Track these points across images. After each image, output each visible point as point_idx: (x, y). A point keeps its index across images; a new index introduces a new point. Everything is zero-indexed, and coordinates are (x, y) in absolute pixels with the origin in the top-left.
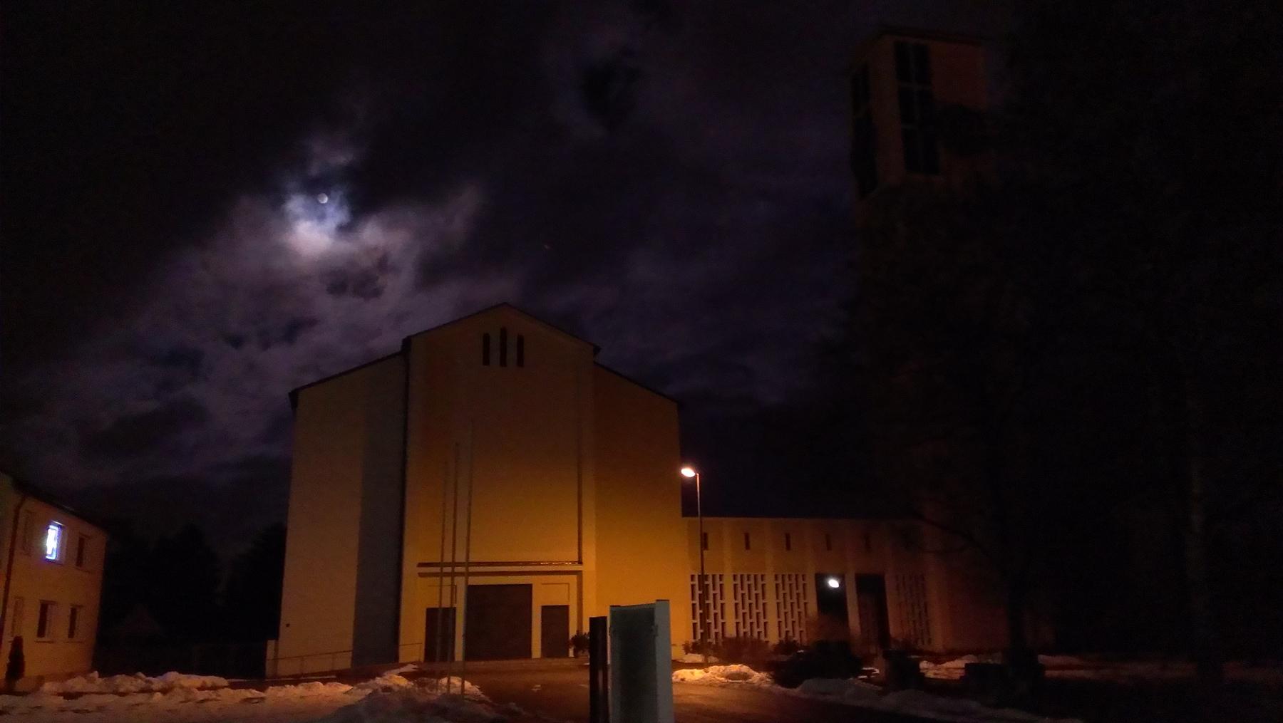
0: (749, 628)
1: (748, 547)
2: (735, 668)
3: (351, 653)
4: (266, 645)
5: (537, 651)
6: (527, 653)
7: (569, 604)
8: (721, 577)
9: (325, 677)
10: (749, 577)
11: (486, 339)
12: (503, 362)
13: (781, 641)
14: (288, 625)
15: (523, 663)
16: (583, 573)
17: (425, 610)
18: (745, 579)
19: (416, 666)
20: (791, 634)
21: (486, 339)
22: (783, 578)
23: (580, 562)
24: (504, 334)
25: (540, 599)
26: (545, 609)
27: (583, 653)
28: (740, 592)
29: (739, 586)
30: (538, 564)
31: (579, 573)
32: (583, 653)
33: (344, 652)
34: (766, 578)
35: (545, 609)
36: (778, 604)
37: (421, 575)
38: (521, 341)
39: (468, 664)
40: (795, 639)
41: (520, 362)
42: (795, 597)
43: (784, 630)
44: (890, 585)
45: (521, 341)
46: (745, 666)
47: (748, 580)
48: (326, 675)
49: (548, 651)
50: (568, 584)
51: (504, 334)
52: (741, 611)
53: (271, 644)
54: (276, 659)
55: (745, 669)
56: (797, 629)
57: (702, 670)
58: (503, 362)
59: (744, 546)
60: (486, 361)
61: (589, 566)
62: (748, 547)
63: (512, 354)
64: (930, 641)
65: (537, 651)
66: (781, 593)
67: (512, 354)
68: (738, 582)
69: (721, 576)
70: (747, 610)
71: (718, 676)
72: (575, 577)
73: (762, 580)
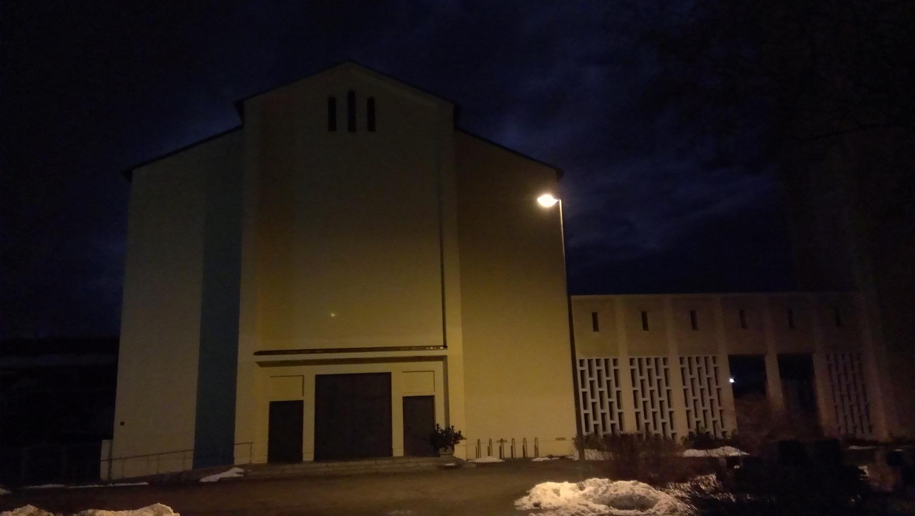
0: (666, 397)
1: (645, 327)
2: (625, 487)
3: (192, 451)
4: (101, 443)
5: (398, 447)
6: (386, 450)
7: (435, 394)
8: (665, 360)
9: (130, 484)
10: (648, 360)
11: (332, 102)
12: (352, 127)
13: (691, 433)
14: (122, 424)
15: (382, 464)
16: (448, 357)
17: (268, 403)
18: (644, 362)
19: (241, 470)
20: (702, 424)
21: (332, 102)
22: (699, 371)
23: (445, 346)
24: (352, 96)
25: (400, 390)
26: (407, 400)
27: (445, 451)
28: (638, 378)
29: (587, 372)
30: (410, 348)
31: (443, 358)
32: (445, 451)
33: (173, 452)
34: (620, 362)
35: (407, 400)
36: (685, 390)
37: (262, 364)
38: (371, 103)
39: (318, 465)
40: (707, 430)
41: (371, 127)
42: (705, 383)
43: (694, 420)
44: (819, 364)
45: (371, 103)
46: (641, 484)
47: (648, 363)
48: (121, 483)
49: (411, 449)
50: (433, 371)
51: (352, 96)
52: (641, 400)
53: (105, 444)
54: (110, 460)
55: (640, 488)
56: (710, 420)
57: (574, 485)
58: (352, 127)
59: (641, 325)
60: (332, 126)
61: (455, 349)
62: (645, 327)
63: (361, 119)
64: (870, 428)
65: (398, 447)
66: (688, 377)
67: (361, 119)
68: (636, 367)
69: (665, 360)
70: (648, 398)
71: (597, 501)
72: (441, 363)
73: (665, 364)
